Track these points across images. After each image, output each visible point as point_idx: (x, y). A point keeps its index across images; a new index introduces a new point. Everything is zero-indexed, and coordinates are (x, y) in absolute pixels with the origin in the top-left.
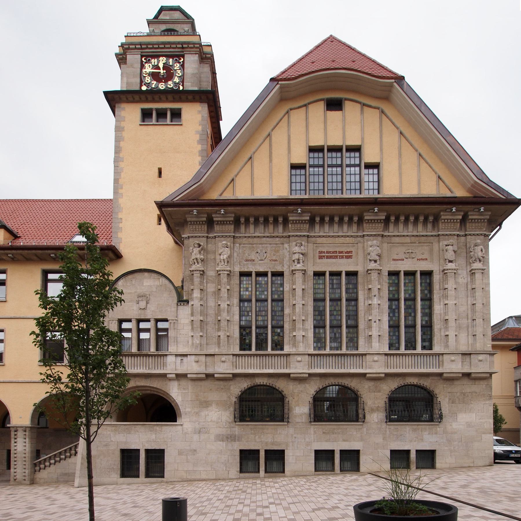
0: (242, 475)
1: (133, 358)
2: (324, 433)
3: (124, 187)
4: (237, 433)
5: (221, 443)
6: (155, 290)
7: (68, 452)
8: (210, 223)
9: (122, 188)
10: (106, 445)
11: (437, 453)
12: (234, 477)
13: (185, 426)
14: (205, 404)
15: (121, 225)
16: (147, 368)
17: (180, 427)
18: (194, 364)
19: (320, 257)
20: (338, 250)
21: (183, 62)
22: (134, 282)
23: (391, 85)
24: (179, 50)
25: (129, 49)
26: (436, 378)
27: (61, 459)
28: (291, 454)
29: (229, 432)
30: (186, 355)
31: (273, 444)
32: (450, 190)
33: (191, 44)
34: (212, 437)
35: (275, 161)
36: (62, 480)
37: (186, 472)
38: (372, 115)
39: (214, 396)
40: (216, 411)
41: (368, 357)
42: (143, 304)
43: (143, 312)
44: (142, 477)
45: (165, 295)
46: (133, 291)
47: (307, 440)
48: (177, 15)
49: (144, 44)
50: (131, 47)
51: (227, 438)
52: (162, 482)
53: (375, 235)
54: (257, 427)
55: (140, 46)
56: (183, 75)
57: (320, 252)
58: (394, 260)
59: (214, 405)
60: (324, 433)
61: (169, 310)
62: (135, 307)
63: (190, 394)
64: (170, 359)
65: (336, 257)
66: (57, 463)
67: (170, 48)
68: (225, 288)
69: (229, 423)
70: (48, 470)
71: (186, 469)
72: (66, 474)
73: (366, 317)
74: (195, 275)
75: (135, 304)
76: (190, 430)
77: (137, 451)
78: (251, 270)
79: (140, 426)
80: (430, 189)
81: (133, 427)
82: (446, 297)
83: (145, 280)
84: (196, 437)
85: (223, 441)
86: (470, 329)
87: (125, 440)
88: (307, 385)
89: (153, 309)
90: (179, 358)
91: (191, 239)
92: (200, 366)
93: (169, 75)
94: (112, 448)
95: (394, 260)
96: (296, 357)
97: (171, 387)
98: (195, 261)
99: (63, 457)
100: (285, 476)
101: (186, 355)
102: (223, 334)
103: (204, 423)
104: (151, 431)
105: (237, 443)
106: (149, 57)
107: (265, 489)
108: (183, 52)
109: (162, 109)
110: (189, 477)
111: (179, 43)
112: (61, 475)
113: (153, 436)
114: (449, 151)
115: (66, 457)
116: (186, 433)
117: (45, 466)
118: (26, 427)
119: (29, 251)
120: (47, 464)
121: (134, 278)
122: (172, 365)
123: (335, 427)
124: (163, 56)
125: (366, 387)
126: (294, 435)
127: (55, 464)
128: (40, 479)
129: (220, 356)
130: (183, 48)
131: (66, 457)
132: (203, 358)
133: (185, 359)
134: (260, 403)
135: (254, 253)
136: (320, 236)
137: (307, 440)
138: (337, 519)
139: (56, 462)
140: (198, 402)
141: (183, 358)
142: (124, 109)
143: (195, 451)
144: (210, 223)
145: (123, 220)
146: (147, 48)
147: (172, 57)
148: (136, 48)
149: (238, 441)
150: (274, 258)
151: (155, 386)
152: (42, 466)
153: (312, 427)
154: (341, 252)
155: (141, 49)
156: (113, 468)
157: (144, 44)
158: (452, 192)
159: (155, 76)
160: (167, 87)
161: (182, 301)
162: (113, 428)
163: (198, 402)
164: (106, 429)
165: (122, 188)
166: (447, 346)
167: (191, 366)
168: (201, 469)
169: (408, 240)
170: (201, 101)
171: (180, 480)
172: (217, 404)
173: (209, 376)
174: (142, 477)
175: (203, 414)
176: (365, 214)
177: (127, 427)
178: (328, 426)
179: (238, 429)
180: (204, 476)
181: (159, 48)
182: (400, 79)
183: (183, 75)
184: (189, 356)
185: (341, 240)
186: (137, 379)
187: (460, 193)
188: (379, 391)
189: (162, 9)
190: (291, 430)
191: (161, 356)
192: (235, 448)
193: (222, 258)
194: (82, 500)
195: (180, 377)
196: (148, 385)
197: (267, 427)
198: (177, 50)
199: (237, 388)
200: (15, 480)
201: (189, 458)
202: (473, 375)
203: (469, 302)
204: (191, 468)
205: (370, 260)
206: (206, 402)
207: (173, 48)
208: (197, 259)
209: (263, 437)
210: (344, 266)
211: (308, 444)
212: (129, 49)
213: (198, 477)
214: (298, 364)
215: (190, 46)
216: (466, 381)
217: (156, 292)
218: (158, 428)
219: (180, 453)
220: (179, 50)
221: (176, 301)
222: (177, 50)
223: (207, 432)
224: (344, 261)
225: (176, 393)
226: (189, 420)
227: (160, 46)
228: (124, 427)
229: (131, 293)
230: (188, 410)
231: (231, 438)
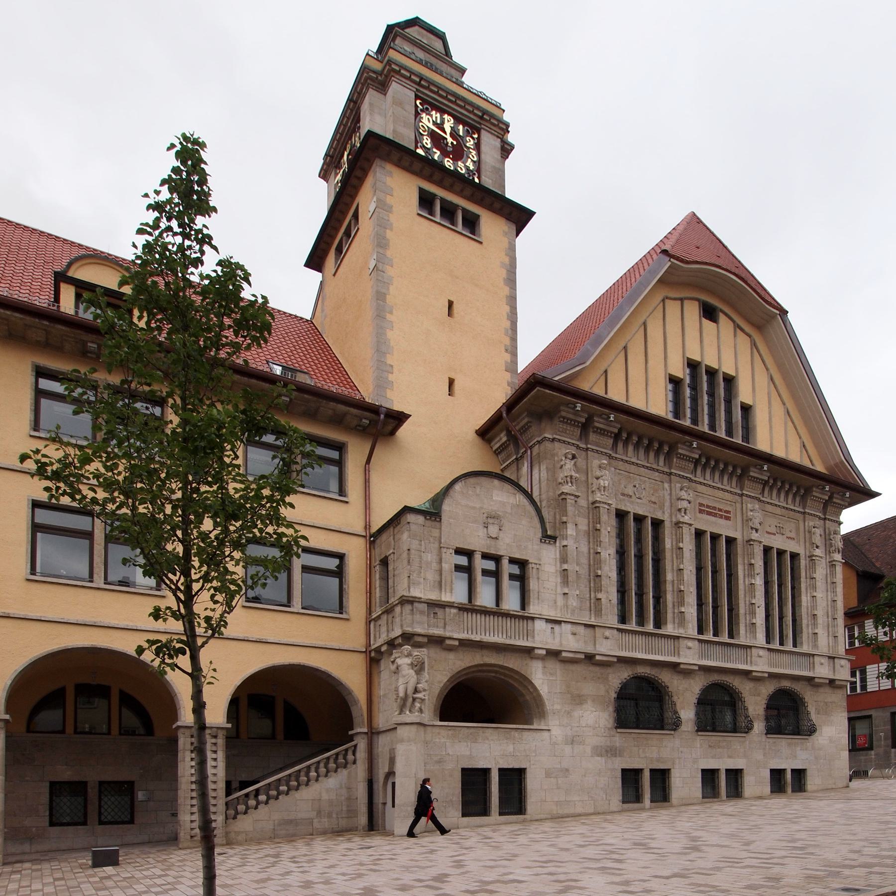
0: (626, 806)
1: (474, 615)
2: (710, 746)
3: (394, 312)
4: (618, 745)
5: (599, 758)
6: (509, 510)
7: (284, 782)
8: (585, 428)
9: (391, 313)
10: (439, 762)
11: (809, 773)
12: (616, 810)
13: (554, 732)
14: (578, 700)
15: (391, 377)
16: (505, 636)
17: (546, 734)
18: (571, 637)
19: (701, 511)
20: (717, 505)
21: (479, 138)
22: (478, 490)
23: (773, 316)
24: (475, 118)
25: (398, 73)
26: (804, 683)
27: (279, 793)
28: (678, 775)
29: (608, 744)
30: (558, 622)
31: (658, 760)
32: (811, 461)
33: (495, 119)
34: (588, 750)
35: (650, 363)
36: (283, 832)
37: (557, 803)
38: (743, 342)
39: (589, 688)
40: (592, 712)
41: (753, 650)
42: (493, 530)
43: (493, 542)
44: (495, 815)
45: (524, 522)
46: (478, 506)
47: (694, 756)
48: (438, 45)
49: (426, 81)
50: (402, 71)
51: (607, 751)
52: (524, 821)
53: (753, 497)
54: (640, 736)
55: (418, 80)
56: (479, 161)
57: (701, 505)
58: (768, 532)
59: (589, 702)
60: (710, 746)
61: (530, 547)
62: (482, 532)
63: (558, 682)
64: (540, 625)
65: (715, 515)
66: (271, 801)
67: (463, 108)
68: (606, 529)
69: (609, 729)
70: (253, 815)
71: (556, 800)
72: (290, 822)
73: (747, 599)
74: (568, 500)
75: (481, 527)
76: (560, 738)
77: (486, 772)
78: (629, 510)
79: (490, 730)
80: (795, 456)
81: (481, 730)
82: (814, 588)
83: (495, 492)
84: (568, 749)
85: (601, 756)
86: (830, 629)
87: (468, 753)
88: (692, 681)
89: (507, 541)
90: (550, 626)
91: (557, 444)
92: (578, 641)
93: (458, 153)
94: (450, 766)
95: (768, 532)
96: (686, 641)
97: (533, 670)
98: (569, 479)
99: (273, 793)
100: (672, 806)
101: (558, 622)
102: (605, 596)
103: (578, 729)
104: (507, 739)
105: (619, 758)
106: (431, 105)
107: (654, 825)
108: (480, 124)
109: (451, 203)
110: (560, 812)
111: (478, 108)
112: (280, 825)
113: (511, 748)
114: (821, 417)
115: (289, 790)
116: (555, 743)
117: (248, 808)
118: (218, 728)
119: (245, 379)
120: (252, 802)
121: (478, 484)
122: (542, 637)
123: (721, 739)
124: (449, 114)
125: (747, 688)
126: (681, 749)
127: (267, 803)
128: (238, 833)
129: (602, 630)
130: (481, 118)
131: (289, 790)
132: (581, 630)
133: (557, 628)
134: (641, 703)
135: (630, 486)
136: (700, 483)
137: (694, 756)
138: (548, 893)
139: (269, 798)
140: (569, 696)
141: (553, 626)
142: (390, 174)
143: (567, 770)
144: (585, 428)
145: (395, 370)
146: (428, 88)
147: (465, 124)
148: (409, 78)
149: (620, 756)
150: (653, 499)
151: (511, 666)
152: (242, 808)
153: (698, 738)
154: (720, 510)
155: (419, 84)
156: (451, 801)
157: (426, 81)
158: (813, 465)
159: (438, 140)
160: (456, 169)
161: (548, 538)
162: (450, 732)
163: (569, 696)
164: (439, 733)
165: (391, 313)
166: (815, 646)
167: (569, 641)
168: (576, 798)
169: (778, 511)
170: (365, 172)
171: (549, 816)
172: (593, 701)
173: (590, 658)
174: (495, 815)
175: (577, 713)
176: (752, 469)
177: (472, 730)
178: (714, 738)
179: (619, 739)
180: (579, 810)
181: (446, 98)
182: (784, 312)
183: (479, 161)
184: (563, 624)
185: (720, 494)
186: (485, 652)
187: (820, 467)
188: (759, 695)
189: (415, 22)
190: (677, 742)
191: (528, 618)
192: (616, 767)
193: (602, 484)
194: (426, 853)
195: (553, 654)
196: (501, 663)
197: (652, 736)
198: (472, 116)
199: (618, 677)
200: (192, 837)
201: (560, 782)
202: (837, 683)
203: (829, 597)
204: (562, 799)
205: (752, 528)
206: (579, 696)
207: (475, 115)
208: (571, 477)
209: (647, 750)
210: (725, 529)
211: (695, 761)
212: (398, 73)
213: (571, 811)
214: (687, 651)
215: (493, 121)
216: (828, 690)
217: (511, 514)
218: (516, 734)
219: (548, 774)
220: (475, 118)
221: (540, 535)
222: (472, 116)
223: (582, 743)
224: (722, 522)
225: (542, 678)
226: (558, 723)
227: (449, 97)
228: (466, 731)
229: (474, 508)
230: (557, 707)
231: (611, 752)
